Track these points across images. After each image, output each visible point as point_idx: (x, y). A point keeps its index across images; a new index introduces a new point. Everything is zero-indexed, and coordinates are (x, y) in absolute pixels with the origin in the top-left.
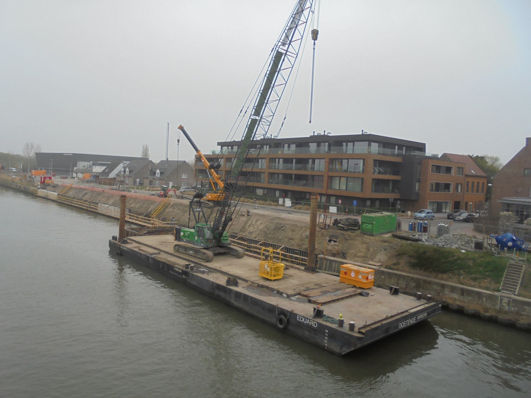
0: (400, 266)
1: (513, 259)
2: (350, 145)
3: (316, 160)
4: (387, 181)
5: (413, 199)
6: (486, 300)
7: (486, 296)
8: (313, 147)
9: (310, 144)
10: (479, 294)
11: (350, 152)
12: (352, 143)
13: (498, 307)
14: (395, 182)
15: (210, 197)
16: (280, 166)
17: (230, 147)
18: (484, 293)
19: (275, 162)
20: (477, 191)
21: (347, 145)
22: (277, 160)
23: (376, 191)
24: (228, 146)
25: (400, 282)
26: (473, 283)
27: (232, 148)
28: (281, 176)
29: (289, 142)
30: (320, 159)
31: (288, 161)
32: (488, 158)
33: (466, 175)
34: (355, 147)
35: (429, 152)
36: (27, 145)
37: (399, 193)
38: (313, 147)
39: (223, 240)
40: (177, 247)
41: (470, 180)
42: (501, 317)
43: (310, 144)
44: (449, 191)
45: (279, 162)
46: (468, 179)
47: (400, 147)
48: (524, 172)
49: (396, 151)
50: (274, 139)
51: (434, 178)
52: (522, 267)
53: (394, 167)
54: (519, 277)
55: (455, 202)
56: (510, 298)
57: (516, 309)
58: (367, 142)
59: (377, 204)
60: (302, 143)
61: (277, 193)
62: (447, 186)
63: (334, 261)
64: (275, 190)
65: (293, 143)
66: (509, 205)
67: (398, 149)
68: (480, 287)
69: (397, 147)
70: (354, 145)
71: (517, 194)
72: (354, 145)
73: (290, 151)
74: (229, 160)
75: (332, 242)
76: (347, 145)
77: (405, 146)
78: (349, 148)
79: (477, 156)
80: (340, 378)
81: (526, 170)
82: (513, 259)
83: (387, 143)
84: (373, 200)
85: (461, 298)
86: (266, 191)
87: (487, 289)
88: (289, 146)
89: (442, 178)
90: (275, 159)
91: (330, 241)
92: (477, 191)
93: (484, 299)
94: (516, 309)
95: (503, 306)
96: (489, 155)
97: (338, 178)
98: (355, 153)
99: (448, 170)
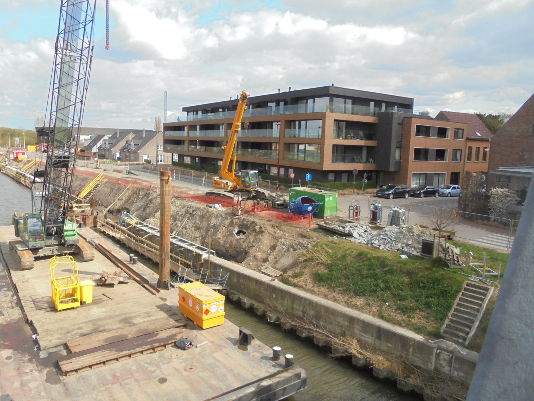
1: (478, 274)
3: (274, 124)
4: (358, 149)
7: (414, 345)
9: (269, 104)
10: (403, 339)
11: (309, 111)
12: (312, 100)
14: (369, 148)
18: (410, 339)
19: (295, 128)
20: (477, 159)
22: (297, 123)
26: (399, 317)
27: (197, 114)
33: (468, 139)
35: (416, 110)
36: (38, 119)
37: (374, 163)
39: (67, 236)
41: (474, 145)
45: (300, 127)
46: (470, 144)
51: (417, 142)
52: (487, 290)
53: (368, 130)
54: (451, 321)
55: (452, 174)
57: (461, 374)
58: (328, 99)
59: (344, 177)
62: (440, 154)
63: (220, 267)
69: (372, 104)
72: (314, 102)
74: (193, 127)
79: (490, 115)
80: (380, 394)
82: (478, 274)
83: (360, 100)
84: (338, 174)
85: (377, 343)
89: (431, 143)
90: (294, 121)
91: (238, 233)
92: (477, 159)
93: (411, 350)
94: (461, 374)
95: (441, 364)
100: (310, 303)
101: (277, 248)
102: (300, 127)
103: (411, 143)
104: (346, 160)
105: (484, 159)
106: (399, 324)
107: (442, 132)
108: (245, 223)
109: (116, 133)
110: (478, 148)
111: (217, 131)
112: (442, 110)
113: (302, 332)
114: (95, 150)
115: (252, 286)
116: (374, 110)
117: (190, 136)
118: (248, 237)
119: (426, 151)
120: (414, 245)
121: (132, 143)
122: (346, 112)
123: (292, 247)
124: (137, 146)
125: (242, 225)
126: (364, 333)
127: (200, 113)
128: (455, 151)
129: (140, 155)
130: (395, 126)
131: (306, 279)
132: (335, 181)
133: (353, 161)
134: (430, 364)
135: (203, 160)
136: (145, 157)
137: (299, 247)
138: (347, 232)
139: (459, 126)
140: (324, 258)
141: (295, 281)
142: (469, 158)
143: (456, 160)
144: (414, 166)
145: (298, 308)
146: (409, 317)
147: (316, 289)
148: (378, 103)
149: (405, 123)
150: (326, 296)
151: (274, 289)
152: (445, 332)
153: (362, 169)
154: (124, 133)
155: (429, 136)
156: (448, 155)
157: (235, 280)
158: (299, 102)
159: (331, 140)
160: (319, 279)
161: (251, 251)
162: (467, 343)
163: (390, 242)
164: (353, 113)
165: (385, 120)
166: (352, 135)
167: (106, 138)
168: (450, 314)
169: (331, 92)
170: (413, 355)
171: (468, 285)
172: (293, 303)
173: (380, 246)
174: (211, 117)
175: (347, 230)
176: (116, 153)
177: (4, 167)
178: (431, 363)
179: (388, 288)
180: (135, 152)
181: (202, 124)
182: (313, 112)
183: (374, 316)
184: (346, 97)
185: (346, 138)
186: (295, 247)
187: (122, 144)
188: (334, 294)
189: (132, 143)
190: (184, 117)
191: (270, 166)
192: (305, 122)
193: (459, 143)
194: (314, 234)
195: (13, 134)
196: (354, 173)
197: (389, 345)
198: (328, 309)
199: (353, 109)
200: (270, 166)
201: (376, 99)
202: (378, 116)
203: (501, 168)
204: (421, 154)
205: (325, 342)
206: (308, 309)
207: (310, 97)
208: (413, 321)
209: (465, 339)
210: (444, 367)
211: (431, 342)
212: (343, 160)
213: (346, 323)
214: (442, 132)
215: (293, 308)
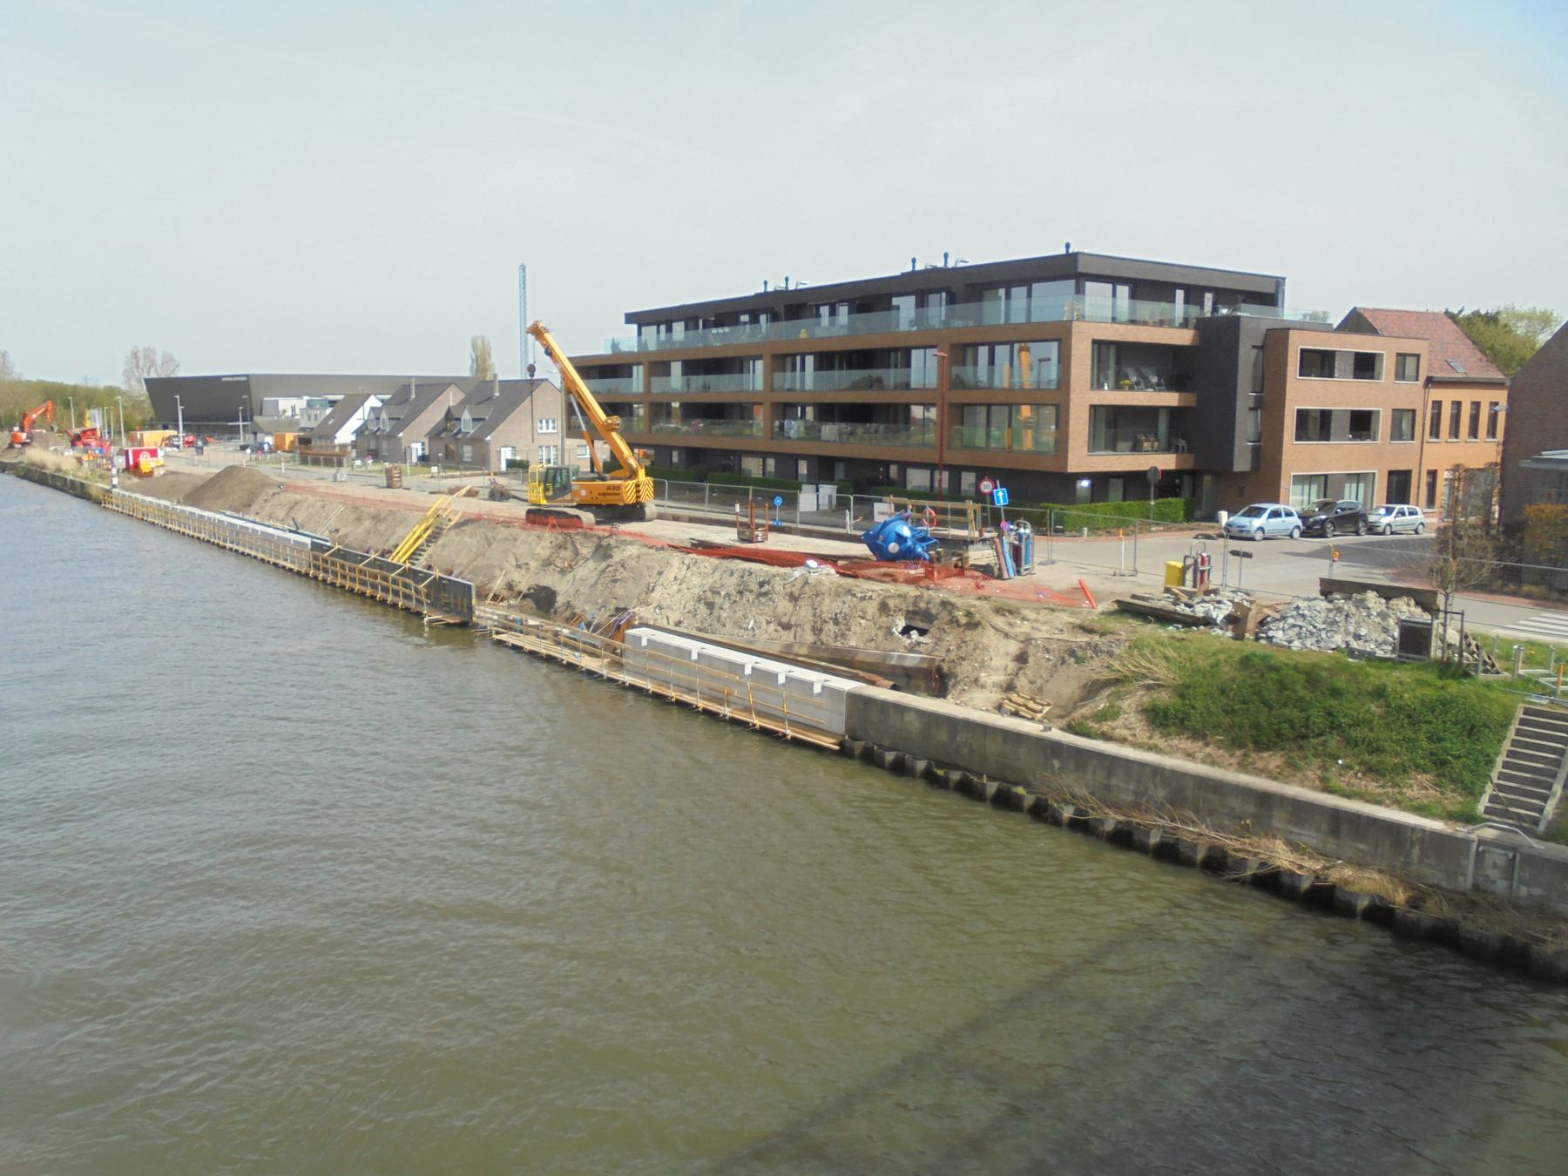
0: (1119, 722)
2: (1019, 292)
3: (914, 353)
4: (1151, 412)
6: (1423, 855)
7: (1422, 841)
8: (906, 306)
9: (895, 301)
10: (1395, 831)
11: (1018, 318)
12: (1024, 289)
13: (1466, 883)
15: (583, 493)
16: (808, 378)
17: (663, 328)
18: (1413, 829)
20: (1474, 432)
21: (1008, 296)
22: (983, 352)
23: (619, 487)
24: (658, 324)
25: (1114, 782)
27: (669, 330)
28: (809, 410)
29: (833, 296)
30: (925, 347)
31: (826, 360)
32: (1520, 317)
33: (1431, 382)
34: (1034, 300)
35: (1292, 309)
36: (135, 355)
37: (1189, 451)
38: (906, 306)
40: (1394, 478)
41: (1447, 396)
42: (1473, 926)
43: (895, 301)
45: (992, 361)
46: (1436, 394)
47: (1194, 294)
49: (1179, 307)
50: (926, 271)
51: (1303, 393)
56: (1514, 849)
58: (1073, 282)
59: (1116, 489)
60: (869, 298)
61: (803, 468)
62: (1361, 424)
65: (842, 301)
67: (1187, 301)
68: (1399, 803)
69: (1180, 294)
70: (1029, 295)
72: (1029, 295)
73: (835, 326)
74: (659, 367)
75: (914, 634)
76: (1008, 296)
78: (1014, 307)
79: (1476, 314)
83: (1149, 286)
84: (1101, 481)
86: (771, 463)
87: (1420, 810)
88: (833, 313)
89: (1339, 394)
90: (794, 356)
91: (906, 631)
92: (1474, 432)
93: (1416, 852)
94: (1537, 891)
96: (1522, 307)
97: (982, 411)
98: (1034, 319)
100: (1157, 771)
101: (1031, 659)
102: (992, 361)
103: (1288, 397)
104: (1121, 445)
105: (1492, 432)
106: (1379, 803)
107: (1365, 366)
108: (923, 605)
109: (407, 388)
110: (1476, 405)
111: (737, 376)
112: (1359, 305)
113: (1147, 833)
114: (345, 435)
115: (993, 746)
116: (1186, 312)
117: (654, 390)
118: (939, 640)
119: (1325, 416)
120: (1374, 636)
121: (466, 416)
122: (1102, 313)
123: (1072, 653)
124: (479, 424)
125: (915, 613)
126: (1295, 825)
127: (679, 327)
128: (1398, 414)
129: (493, 449)
130: (1247, 357)
131: (1130, 718)
132: (1092, 500)
133: (1136, 448)
134: (1461, 879)
135: (694, 455)
136: (507, 454)
137: (1089, 653)
138: (1200, 615)
139: (1408, 346)
140: (1162, 671)
141: (1105, 727)
142: (1435, 432)
143: (1400, 437)
144: (1299, 457)
145: (1123, 785)
146: (1395, 785)
147: (1161, 743)
148: (1194, 294)
149: (1276, 340)
150: (1190, 756)
151: (1056, 748)
152: (1488, 811)
153: (1172, 466)
154: (431, 388)
155: (1331, 375)
156: (1383, 425)
157: (943, 735)
158: (987, 294)
159: (1084, 396)
160: (1158, 718)
161: (958, 670)
162: (1542, 828)
163: (1312, 634)
164: (1133, 322)
165: (1218, 338)
166: (1134, 379)
167: (373, 402)
168: (1494, 775)
169: (1081, 269)
170: (1421, 862)
171: (1527, 711)
172: (1109, 776)
173: (1290, 642)
174: (718, 339)
175: (1200, 611)
176: (414, 445)
177: (109, 491)
178: (1465, 875)
179: (1335, 727)
180: (477, 441)
181: (694, 357)
182: (1029, 322)
183: (1315, 788)
184: (1115, 280)
185: (1118, 387)
186: (1080, 653)
187: (433, 416)
188: (1208, 750)
189: (466, 416)
190: (629, 339)
191: (904, 466)
192: (1007, 347)
193: (1411, 394)
194: (1112, 624)
195: (87, 398)
196: (1150, 476)
197: (1361, 846)
198: (1201, 782)
199: (1132, 310)
200: (904, 466)
201: (1220, 285)
202: (1196, 328)
203: (1547, 454)
204: (1316, 425)
205: (1212, 848)
206: (1151, 786)
207: (1020, 283)
208: (1409, 793)
209: (1536, 822)
210: (1493, 882)
211: (1461, 830)
212: (1112, 446)
213: (1251, 808)
214: (1365, 366)
215: (1108, 788)
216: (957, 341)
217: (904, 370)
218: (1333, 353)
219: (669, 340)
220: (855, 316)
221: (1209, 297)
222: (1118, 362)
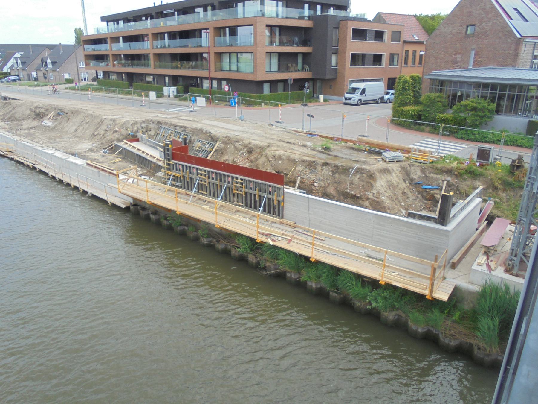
4: (294, 55)
5: (328, 77)
14: (305, 55)
17: (115, 23)
20: (414, 63)
27: (118, 23)
33: (405, 42)
34: (246, 7)
37: (310, 71)
41: (411, 48)
44: (380, 65)
48: (467, 30)
49: (306, 12)
51: (356, 47)
62: (377, 59)
64: (165, 76)
66: (442, 83)
67: (309, 9)
70: (244, 5)
71: (454, 64)
72: (244, 5)
74: (115, 39)
77: (319, 4)
81: (469, 28)
89: (368, 47)
99: (379, 35)
103: (348, 48)
111: (141, 43)
128: (392, 56)
142: (406, 63)
156: (385, 60)
174: (135, 28)
190: (103, 28)
203: (434, 72)
214: (379, 35)
216: (215, 27)
217: (162, 41)
218: (366, 30)
219: (118, 28)
220: (335, 11)
221: (319, 7)
222: (280, 34)
